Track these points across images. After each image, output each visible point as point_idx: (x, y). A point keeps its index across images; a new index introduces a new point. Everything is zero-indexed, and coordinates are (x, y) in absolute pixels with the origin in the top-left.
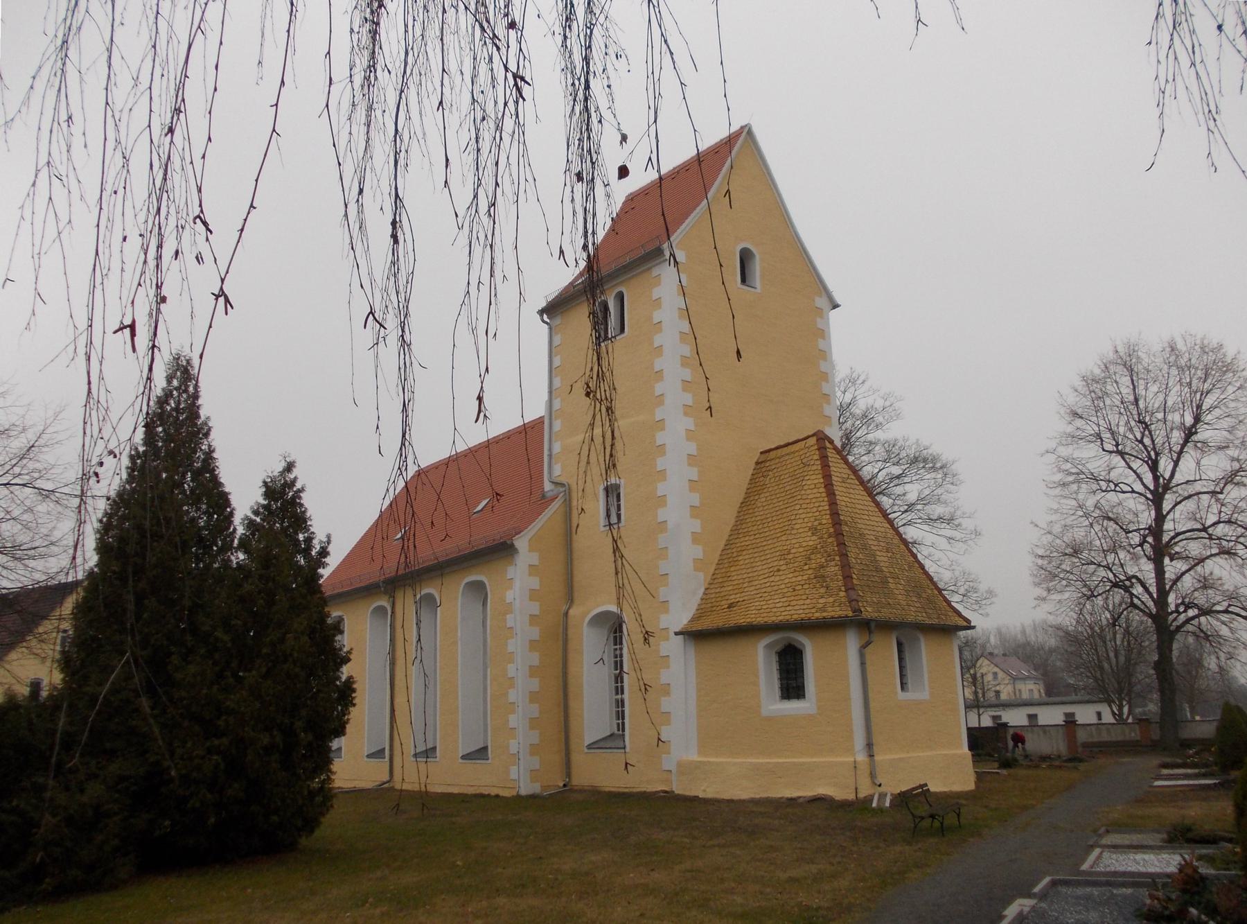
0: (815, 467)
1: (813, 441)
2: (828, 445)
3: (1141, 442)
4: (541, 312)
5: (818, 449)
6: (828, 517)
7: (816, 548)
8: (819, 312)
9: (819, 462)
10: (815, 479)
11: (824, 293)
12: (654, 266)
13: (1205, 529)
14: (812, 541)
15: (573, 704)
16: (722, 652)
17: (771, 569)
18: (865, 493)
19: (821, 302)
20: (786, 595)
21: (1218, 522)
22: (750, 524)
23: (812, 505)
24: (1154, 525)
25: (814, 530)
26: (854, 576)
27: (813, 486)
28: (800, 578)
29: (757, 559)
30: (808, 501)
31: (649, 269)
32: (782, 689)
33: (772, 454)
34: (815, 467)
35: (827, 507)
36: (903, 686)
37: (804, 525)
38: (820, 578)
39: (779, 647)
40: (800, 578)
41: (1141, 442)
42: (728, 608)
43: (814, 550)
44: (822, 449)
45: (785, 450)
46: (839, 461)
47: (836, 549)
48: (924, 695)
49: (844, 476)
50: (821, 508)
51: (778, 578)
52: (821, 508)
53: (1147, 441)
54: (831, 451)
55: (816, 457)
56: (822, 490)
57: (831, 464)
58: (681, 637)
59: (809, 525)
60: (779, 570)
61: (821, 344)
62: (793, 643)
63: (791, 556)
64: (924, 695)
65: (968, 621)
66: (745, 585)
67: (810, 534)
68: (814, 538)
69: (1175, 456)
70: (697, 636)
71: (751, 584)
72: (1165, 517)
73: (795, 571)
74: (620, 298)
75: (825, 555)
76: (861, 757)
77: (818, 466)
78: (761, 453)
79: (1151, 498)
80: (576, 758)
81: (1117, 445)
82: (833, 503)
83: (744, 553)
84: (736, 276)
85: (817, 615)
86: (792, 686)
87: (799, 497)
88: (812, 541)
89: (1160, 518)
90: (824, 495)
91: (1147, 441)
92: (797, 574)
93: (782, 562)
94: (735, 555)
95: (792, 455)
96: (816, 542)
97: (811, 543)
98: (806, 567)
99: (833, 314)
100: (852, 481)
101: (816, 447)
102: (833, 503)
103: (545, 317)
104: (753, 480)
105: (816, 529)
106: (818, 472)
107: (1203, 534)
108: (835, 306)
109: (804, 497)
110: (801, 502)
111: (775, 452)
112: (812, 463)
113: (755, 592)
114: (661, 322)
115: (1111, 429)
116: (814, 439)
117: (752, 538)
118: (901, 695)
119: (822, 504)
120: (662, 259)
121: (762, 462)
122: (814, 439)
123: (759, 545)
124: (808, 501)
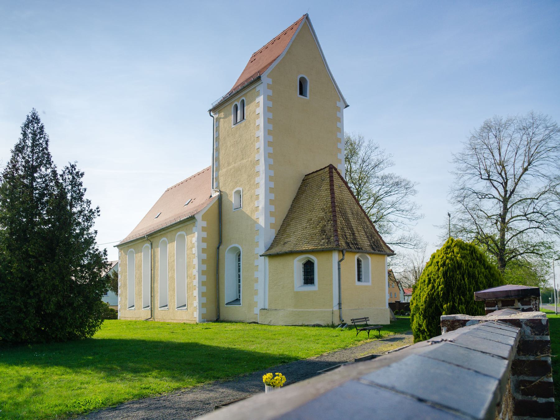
0: (327, 181)
1: (327, 169)
2: (334, 171)
3: (500, 174)
4: (210, 111)
5: (329, 173)
6: (330, 204)
7: (323, 218)
8: (339, 110)
9: (329, 179)
10: (326, 186)
11: (341, 100)
12: (258, 86)
13: (525, 215)
14: (322, 214)
15: (221, 286)
16: (279, 263)
17: (303, 227)
18: (350, 193)
19: (340, 104)
20: (308, 239)
21: (533, 212)
22: (297, 208)
23: (324, 198)
24: (502, 214)
25: (323, 210)
26: (339, 230)
27: (325, 190)
28: (315, 231)
29: (298, 223)
30: (322, 197)
31: (255, 87)
32: (305, 279)
33: (310, 176)
34: (327, 181)
35: (330, 199)
36: (359, 279)
37: (319, 207)
38: (323, 231)
39: (304, 261)
40: (315, 231)
41: (500, 174)
42: (283, 245)
43: (322, 219)
44: (331, 172)
45: (315, 174)
46: (339, 178)
47: (332, 218)
48: (369, 284)
49: (340, 185)
50: (327, 200)
51: (305, 231)
52: (327, 200)
53: (503, 174)
54: (335, 174)
55: (328, 176)
56: (329, 191)
57: (334, 180)
58: (263, 257)
59: (322, 207)
60: (306, 228)
61: (339, 125)
62: (310, 260)
63: (312, 222)
64: (369, 284)
65: (393, 251)
66: (292, 235)
67: (321, 211)
68: (323, 213)
69: (516, 181)
70: (271, 255)
71: (294, 234)
72: (508, 210)
73: (313, 228)
74: (243, 102)
75: (327, 221)
76: (336, 308)
77: (328, 180)
78: (306, 176)
79: (502, 200)
80: (222, 309)
81: (489, 176)
82: (333, 198)
83: (293, 220)
84: (297, 91)
85: (319, 247)
86: (309, 278)
87: (319, 195)
88: (322, 214)
89: (506, 210)
90: (330, 194)
91: (503, 174)
92: (313, 229)
93: (308, 224)
94: (289, 222)
95: (318, 177)
96: (323, 215)
97: (321, 216)
98: (318, 226)
99: (345, 110)
100: (344, 188)
101: (328, 172)
102: (333, 198)
103: (212, 114)
104: (300, 188)
105: (324, 209)
106: (328, 183)
107: (525, 218)
108: (347, 106)
109: (321, 195)
110: (319, 197)
111: (311, 175)
112: (326, 179)
113: (295, 237)
114: (259, 113)
115: (487, 170)
116: (328, 168)
117: (297, 214)
118: (358, 283)
119: (328, 198)
120: (261, 82)
121: (305, 180)
122: (328, 168)
123: (299, 217)
124: (322, 197)
